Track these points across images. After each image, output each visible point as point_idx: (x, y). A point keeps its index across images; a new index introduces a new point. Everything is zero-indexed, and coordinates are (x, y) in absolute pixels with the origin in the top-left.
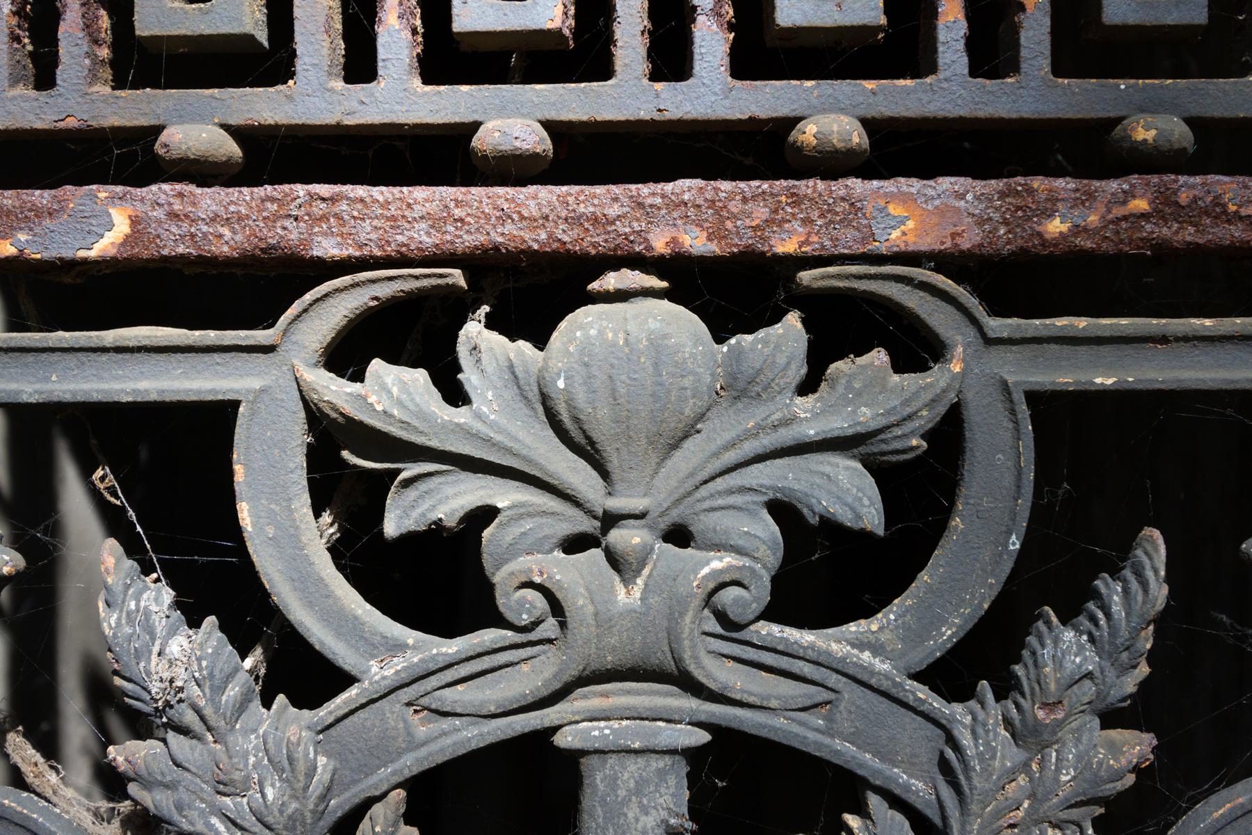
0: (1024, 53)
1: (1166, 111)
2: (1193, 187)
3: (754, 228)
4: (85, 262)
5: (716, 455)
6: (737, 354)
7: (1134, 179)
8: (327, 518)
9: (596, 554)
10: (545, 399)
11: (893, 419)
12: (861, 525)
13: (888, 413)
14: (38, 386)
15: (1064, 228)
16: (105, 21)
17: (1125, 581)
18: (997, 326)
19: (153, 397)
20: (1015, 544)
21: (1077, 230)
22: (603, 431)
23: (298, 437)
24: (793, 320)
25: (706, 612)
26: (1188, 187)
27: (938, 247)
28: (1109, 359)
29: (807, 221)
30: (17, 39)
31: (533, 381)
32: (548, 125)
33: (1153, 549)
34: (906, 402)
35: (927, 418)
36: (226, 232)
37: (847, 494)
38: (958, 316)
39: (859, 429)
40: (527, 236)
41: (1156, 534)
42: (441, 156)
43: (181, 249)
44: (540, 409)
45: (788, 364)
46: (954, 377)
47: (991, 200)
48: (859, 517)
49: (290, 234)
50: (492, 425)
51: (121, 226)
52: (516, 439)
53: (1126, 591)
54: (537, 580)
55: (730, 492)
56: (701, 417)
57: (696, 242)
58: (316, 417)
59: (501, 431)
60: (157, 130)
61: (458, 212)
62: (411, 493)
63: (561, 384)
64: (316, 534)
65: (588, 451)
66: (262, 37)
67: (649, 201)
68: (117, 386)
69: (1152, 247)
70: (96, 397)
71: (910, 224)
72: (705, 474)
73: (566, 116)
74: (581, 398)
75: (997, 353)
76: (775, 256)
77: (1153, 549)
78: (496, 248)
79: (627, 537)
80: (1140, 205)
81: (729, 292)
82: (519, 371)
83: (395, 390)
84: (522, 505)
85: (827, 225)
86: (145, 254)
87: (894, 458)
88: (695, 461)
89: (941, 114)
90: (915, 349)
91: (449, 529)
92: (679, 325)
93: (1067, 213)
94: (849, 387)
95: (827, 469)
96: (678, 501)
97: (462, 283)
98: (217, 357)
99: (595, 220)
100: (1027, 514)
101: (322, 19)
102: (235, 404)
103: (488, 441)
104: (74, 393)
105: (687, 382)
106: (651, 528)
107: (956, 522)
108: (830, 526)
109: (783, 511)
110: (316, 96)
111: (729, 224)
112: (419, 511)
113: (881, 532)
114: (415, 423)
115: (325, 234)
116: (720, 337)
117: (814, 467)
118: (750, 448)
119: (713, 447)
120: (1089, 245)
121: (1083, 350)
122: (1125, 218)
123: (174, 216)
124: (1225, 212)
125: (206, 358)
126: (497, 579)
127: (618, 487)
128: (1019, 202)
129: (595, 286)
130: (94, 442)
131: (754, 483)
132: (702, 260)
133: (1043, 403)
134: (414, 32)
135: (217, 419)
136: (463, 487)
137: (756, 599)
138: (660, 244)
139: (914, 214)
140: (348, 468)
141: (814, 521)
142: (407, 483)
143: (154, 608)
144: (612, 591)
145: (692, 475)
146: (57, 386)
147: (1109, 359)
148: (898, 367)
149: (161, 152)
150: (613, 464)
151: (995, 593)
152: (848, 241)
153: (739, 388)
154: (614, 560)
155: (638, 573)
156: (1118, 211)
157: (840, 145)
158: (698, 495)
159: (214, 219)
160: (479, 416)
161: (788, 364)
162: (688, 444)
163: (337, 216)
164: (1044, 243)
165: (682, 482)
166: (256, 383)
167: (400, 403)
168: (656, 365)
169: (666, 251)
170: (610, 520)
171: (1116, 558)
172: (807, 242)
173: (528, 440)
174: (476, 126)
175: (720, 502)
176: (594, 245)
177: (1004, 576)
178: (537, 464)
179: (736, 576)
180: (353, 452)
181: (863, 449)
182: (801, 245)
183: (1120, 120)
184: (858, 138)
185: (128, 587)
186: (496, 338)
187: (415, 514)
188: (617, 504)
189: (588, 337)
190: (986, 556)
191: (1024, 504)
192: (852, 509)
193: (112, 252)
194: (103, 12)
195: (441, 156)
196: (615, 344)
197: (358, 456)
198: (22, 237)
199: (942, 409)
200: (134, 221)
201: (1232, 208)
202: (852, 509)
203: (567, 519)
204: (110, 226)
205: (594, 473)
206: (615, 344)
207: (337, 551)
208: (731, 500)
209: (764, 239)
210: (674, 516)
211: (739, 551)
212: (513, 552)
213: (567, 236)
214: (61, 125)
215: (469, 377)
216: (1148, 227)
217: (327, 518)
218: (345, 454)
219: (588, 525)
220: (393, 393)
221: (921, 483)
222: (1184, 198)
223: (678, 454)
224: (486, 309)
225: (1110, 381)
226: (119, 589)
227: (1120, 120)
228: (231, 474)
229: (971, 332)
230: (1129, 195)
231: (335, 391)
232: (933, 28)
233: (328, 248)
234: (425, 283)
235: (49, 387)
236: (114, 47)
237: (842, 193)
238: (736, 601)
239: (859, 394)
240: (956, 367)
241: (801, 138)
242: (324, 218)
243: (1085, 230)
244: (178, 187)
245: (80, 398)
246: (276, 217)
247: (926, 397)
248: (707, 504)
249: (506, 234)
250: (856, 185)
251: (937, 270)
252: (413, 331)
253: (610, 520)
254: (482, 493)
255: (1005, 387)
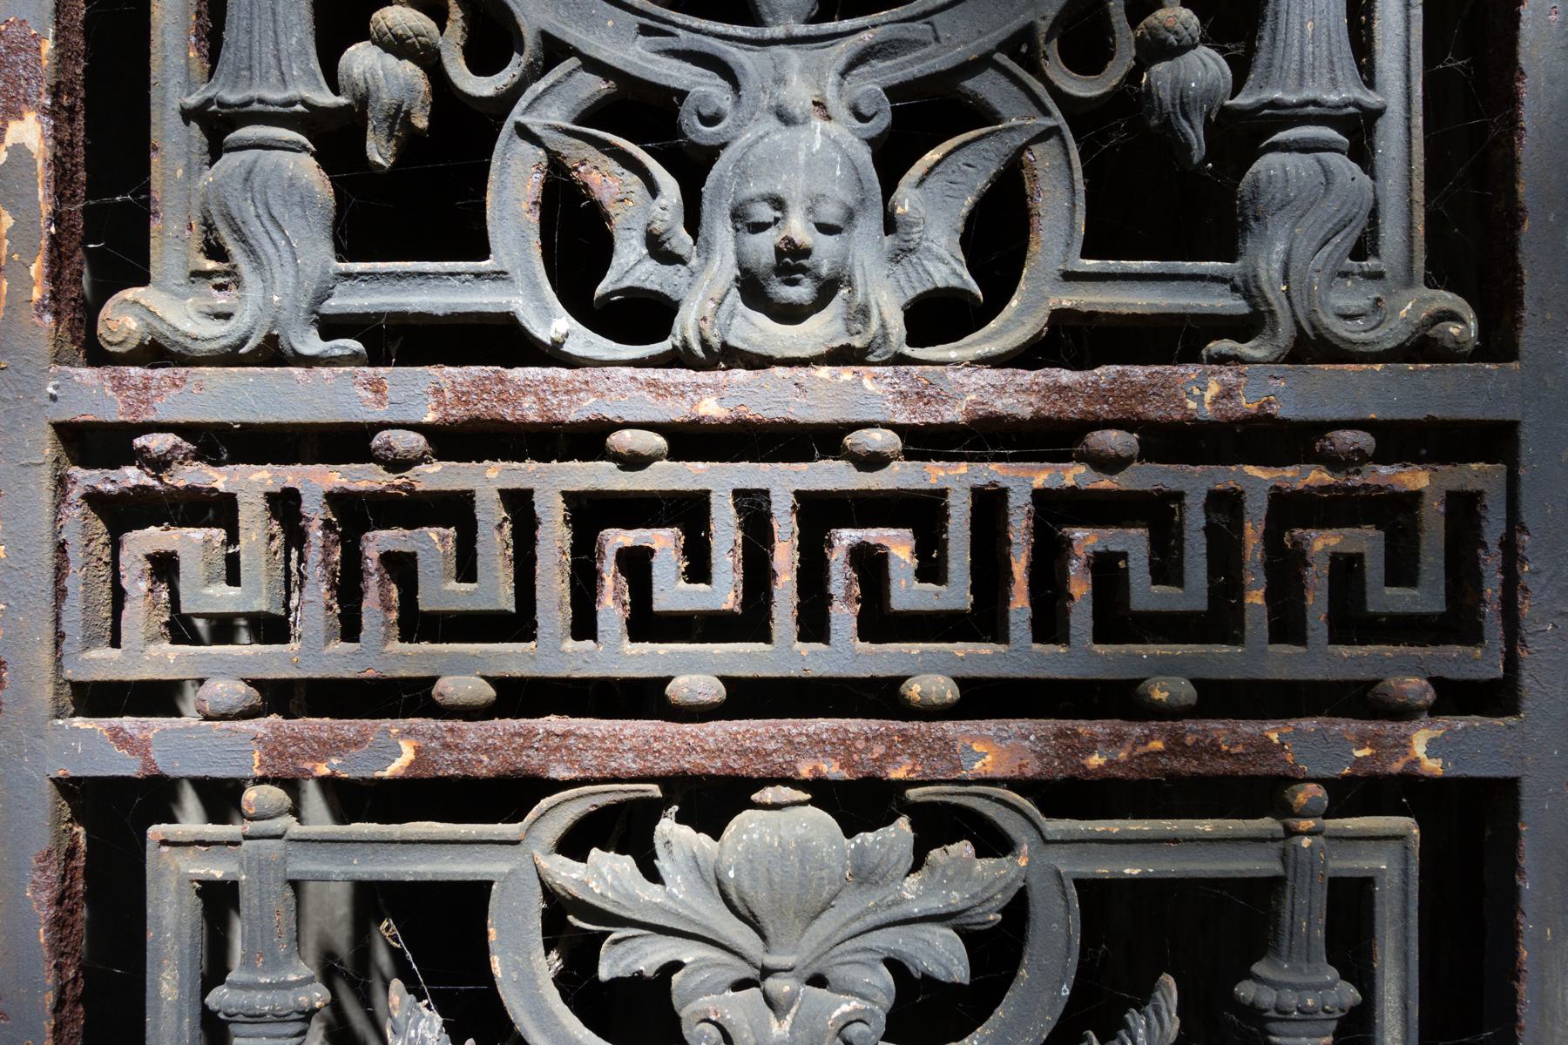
0: (1072, 631)
1: (1176, 674)
2: (1196, 732)
3: (874, 760)
4: (380, 780)
5: (845, 925)
6: (861, 851)
7: (1153, 724)
8: (554, 955)
9: (755, 990)
10: (719, 883)
11: (976, 902)
12: (952, 980)
13: (973, 897)
14: (343, 868)
15: (1102, 761)
16: (395, 593)
17: (1147, 1017)
18: (1056, 827)
19: (429, 877)
20: (1066, 991)
21: (1110, 763)
22: (761, 903)
23: (537, 904)
24: (903, 823)
25: (838, 1040)
26: (1192, 729)
27: (1009, 775)
28: (1132, 849)
29: (913, 755)
30: (330, 608)
31: (711, 869)
32: (725, 680)
33: (1168, 990)
34: (985, 889)
35: (1001, 900)
36: (485, 758)
37: (943, 955)
38: (1024, 822)
39: (951, 909)
40: (707, 763)
41: (1171, 981)
42: (642, 698)
43: (451, 771)
44: (716, 889)
45: (898, 861)
46: (1021, 870)
47: (1048, 740)
48: (950, 974)
49: (532, 760)
50: (682, 902)
51: (408, 754)
52: (697, 912)
53: (1148, 1025)
54: (713, 1018)
55: (856, 951)
56: (835, 897)
57: (832, 770)
58: (549, 893)
59: (688, 907)
60: (433, 680)
61: (656, 746)
62: (620, 949)
63: (731, 874)
64: (547, 965)
65: (752, 921)
66: (511, 607)
67: (797, 740)
68: (402, 868)
69: (1167, 776)
70: (387, 877)
71: (989, 758)
72: (837, 939)
73: (736, 673)
74: (746, 884)
75: (1052, 849)
76: (889, 781)
77: (1168, 990)
78: (684, 772)
79: (780, 986)
80: (1157, 745)
81: (857, 803)
82: (700, 861)
83: (609, 878)
84: (703, 959)
85: (927, 758)
86: (426, 775)
87: (977, 928)
88: (830, 929)
89: (1012, 675)
90: (993, 842)
91: (648, 979)
92: (818, 823)
93: (1104, 749)
94: (944, 875)
95: (927, 936)
96: (818, 958)
97: (659, 794)
98: (477, 848)
99: (757, 753)
100: (1075, 969)
101: (557, 600)
102: (491, 883)
103: (678, 915)
104: (370, 874)
105: (825, 873)
106: (796, 977)
107: (1023, 972)
108: (928, 980)
109: (895, 966)
110: (553, 653)
111: (856, 757)
112: (629, 960)
113: (967, 982)
114: (623, 902)
115: (558, 761)
116: (849, 833)
117: (918, 934)
118: (871, 920)
119: (843, 919)
120: (1120, 774)
121: (1116, 847)
122: (1146, 754)
123: (446, 746)
124: (1219, 749)
125: (469, 848)
126: (683, 1014)
127: (774, 947)
128: (1069, 742)
129: (756, 797)
130: (381, 900)
131: (874, 945)
132: (836, 783)
133: (1086, 886)
134: (624, 604)
135: (476, 893)
136: (658, 946)
137: (874, 1032)
138: (805, 771)
139: (992, 749)
140: (571, 929)
141: (918, 976)
142: (616, 942)
143: (429, 1035)
144: (768, 1026)
145: (827, 939)
146: (358, 868)
147: (1132, 849)
148: (980, 854)
149: (438, 698)
150: (770, 930)
151: (1051, 1027)
152: (942, 768)
153: (864, 875)
154: (769, 1001)
155: (788, 1011)
156: (1141, 750)
157: (937, 701)
158: (832, 953)
159: (476, 749)
160: (671, 896)
161: (898, 861)
162: (825, 916)
163: (566, 747)
164: (1087, 772)
165: (819, 944)
166: (505, 868)
167: (613, 888)
168: (801, 861)
169: (809, 776)
170: (767, 972)
171: (1142, 996)
172: (913, 771)
173: (707, 913)
174: (669, 679)
175: (849, 958)
176: (757, 771)
177: (1058, 1016)
178: (714, 931)
179: (860, 1016)
180: (576, 917)
181: (954, 921)
182: (909, 772)
183: (1142, 680)
184: (951, 693)
185: (408, 1018)
186: (686, 831)
187: (623, 964)
188: (771, 961)
189: (751, 839)
190: (1045, 998)
191: (1073, 961)
192: (946, 968)
193: (401, 773)
194: (394, 586)
195: (642, 698)
196: (771, 846)
197: (581, 919)
198: (335, 761)
199: (1012, 893)
200: (418, 751)
201: (1225, 748)
202: (946, 968)
203: (734, 969)
204: (400, 754)
205: (756, 935)
206: (771, 846)
207: (560, 980)
208: (857, 957)
209: (881, 768)
210: (814, 969)
211: (863, 997)
212: (696, 993)
213: (737, 765)
214: (363, 675)
215: (663, 864)
216: (1164, 761)
217: (554, 955)
218: (570, 918)
219: (752, 973)
220: (605, 876)
221: (997, 946)
222: (1189, 740)
223: (817, 923)
224: (676, 808)
225: (1136, 872)
226: (403, 1020)
227: (1142, 680)
228: (486, 934)
229: (1034, 834)
230: (1149, 738)
231: (568, 874)
232: (1007, 612)
233: (559, 772)
234: (632, 795)
235: (351, 869)
236: (401, 610)
237: (939, 734)
238: (859, 1035)
239: (951, 880)
240: (1023, 862)
241: (909, 693)
242: (558, 749)
243: (1117, 763)
244: (449, 723)
245: (375, 878)
246: (522, 748)
247: (1000, 885)
248: (839, 960)
249: (691, 763)
250: (948, 725)
251: (1009, 788)
252: (622, 828)
253: (767, 972)
254: (673, 951)
255: (1058, 873)
